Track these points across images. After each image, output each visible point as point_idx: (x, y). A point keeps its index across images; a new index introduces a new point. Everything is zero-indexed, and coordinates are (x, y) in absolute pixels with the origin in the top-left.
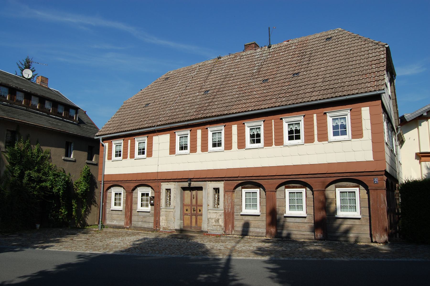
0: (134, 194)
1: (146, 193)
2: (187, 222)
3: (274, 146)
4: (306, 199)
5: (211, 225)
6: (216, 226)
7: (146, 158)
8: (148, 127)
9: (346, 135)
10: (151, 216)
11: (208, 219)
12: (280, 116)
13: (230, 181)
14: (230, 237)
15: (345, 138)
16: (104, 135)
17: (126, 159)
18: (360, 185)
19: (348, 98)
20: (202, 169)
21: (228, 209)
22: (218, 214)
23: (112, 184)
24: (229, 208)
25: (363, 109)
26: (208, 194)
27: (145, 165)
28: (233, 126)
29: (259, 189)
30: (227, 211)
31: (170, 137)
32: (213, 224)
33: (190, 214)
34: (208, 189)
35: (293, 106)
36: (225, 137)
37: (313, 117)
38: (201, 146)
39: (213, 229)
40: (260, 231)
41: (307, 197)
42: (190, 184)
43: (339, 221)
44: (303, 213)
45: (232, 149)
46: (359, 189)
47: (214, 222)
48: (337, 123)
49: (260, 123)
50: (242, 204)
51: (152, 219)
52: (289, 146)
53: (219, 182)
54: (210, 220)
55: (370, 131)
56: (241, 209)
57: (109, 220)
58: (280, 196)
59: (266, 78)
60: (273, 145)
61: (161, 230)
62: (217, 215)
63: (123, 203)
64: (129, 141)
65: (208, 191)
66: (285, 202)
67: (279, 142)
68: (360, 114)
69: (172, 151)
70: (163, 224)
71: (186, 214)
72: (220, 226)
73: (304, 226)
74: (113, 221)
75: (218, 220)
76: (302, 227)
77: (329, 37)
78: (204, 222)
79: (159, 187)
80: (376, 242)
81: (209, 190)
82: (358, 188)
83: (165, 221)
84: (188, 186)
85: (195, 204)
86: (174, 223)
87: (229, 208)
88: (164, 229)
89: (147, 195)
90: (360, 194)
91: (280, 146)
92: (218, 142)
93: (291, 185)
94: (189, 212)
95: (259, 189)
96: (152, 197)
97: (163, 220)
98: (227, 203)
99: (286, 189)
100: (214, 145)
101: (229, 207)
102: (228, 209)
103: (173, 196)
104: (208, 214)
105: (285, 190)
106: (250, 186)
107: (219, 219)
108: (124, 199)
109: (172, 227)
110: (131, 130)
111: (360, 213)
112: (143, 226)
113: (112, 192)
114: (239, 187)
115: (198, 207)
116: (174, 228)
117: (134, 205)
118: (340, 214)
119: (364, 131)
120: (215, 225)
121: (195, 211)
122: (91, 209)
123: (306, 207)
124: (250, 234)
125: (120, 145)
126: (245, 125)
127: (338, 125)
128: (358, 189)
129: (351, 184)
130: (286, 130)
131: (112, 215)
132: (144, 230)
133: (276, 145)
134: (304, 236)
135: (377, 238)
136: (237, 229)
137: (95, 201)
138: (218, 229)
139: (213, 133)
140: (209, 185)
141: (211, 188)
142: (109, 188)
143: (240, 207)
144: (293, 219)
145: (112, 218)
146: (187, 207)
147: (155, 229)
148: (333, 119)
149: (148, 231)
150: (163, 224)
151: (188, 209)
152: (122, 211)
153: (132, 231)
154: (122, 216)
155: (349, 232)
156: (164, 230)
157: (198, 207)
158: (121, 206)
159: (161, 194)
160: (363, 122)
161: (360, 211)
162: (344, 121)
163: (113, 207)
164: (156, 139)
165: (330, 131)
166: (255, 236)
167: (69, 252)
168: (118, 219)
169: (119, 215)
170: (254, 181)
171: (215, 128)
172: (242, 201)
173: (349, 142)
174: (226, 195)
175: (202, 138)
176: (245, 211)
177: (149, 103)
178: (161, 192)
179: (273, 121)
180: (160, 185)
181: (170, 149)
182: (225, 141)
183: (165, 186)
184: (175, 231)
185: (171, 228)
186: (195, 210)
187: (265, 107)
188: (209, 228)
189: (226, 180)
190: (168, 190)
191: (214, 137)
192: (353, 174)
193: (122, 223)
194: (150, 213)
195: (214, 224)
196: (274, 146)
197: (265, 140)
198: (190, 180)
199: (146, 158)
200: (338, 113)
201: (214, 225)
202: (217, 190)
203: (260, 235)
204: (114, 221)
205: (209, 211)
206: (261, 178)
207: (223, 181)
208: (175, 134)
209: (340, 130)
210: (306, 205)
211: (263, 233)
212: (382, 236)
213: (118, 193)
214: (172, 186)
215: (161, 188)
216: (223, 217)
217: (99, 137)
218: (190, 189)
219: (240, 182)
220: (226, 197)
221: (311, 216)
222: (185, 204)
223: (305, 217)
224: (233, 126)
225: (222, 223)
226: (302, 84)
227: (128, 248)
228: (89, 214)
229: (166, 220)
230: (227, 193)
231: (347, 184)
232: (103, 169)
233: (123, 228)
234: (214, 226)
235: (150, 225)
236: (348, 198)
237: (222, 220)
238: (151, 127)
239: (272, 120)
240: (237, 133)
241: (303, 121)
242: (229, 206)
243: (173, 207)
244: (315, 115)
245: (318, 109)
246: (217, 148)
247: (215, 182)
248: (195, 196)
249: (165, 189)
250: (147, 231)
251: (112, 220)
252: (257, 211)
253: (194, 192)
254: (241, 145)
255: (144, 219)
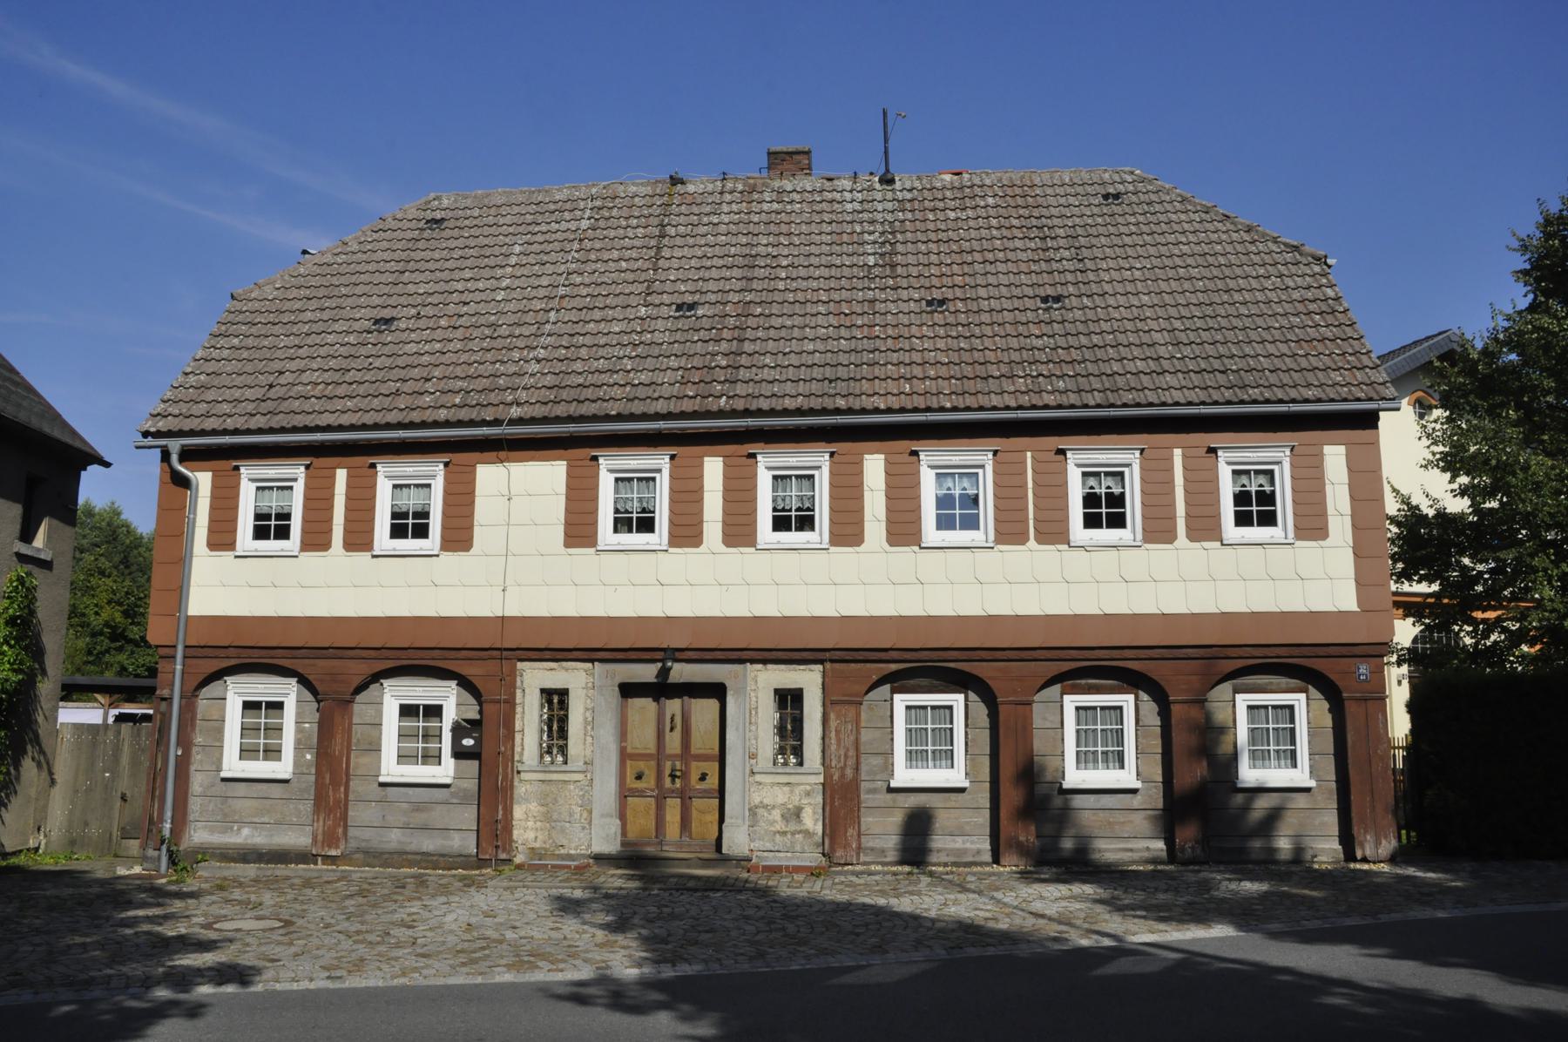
0: (356, 708)
1: (425, 706)
2: (643, 822)
3: (1032, 543)
4: (1136, 730)
5: (766, 831)
6: (789, 836)
7: (438, 556)
8: (447, 424)
9: (978, 528)
10: (455, 801)
11: (753, 811)
12: (1213, 439)
13: (853, 665)
14: (857, 874)
15: (1272, 537)
16: (192, 433)
17: (857, 548)
18: (1310, 687)
19: (1294, 411)
20: (728, 615)
21: (843, 769)
22: (798, 790)
23: (233, 662)
24: (845, 765)
25: (1327, 449)
26: (753, 712)
27: (486, 583)
28: (706, 459)
29: (962, 696)
30: (836, 777)
31: (569, 476)
32: (773, 829)
33: (653, 790)
34: (753, 694)
35: (1112, 413)
36: (306, 508)
37: (1170, 459)
38: (720, 524)
39: (776, 848)
40: (968, 845)
41: (1141, 723)
42: (664, 672)
43: (1239, 799)
44: (1125, 777)
45: (863, 546)
46: (1308, 699)
47: (778, 818)
48: (1244, 486)
49: (980, 458)
50: (892, 750)
51: (467, 816)
52: (1088, 549)
53: (802, 667)
54: (761, 811)
55: (1348, 521)
56: (889, 769)
57: (206, 827)
58: (1045, 719)
59: (387, 313)
60: (1028, 540)
61: (519, 859)
62: (792, 792)
63: (295, 748)
64: (341, 475)
65: (754, 699)
66: (1063, 740)
67: (1053, 532)
68: (860, 473)
69: (579, 531)
70: (531, 835)
71: (640, 794)
72: (807, 834)
73: (1131, 822)
74: (232, 828)
75: (797, 813)
76: (1123, 823)
77: (439, 217)
78: (733, 821)
79: (509, 684)
80: (1365, 860)
81: (757, 697)
82: (1304, 695)
83: (539, 824)
84: (655, 681)
85: (678, 751)
86: (584, 828)
87: (845, 765)
88: (535, 854)
89: (434, 711)
90: (1308, 712)
91: (1202, 543)
92: (797, 510)
93: (1083, 682)
94: (649, 782)
95: (962, 696)
96: (464, 720)
97: (527, 820)
98: (839, 744)
99: (1065, 697)
100: (781, 524)
101: (845, 761)
102: (843, 769)
103: (581, 719)
104: (752, 790)
105: (1062, 698)
106: (924, 682)
107: (803, 808)
108: (299, 730)
109: (573, 845)
110: (527, 420)
111: (1311, 772)
112: (413, 847)
113: (230, 695)
114: (881, 688)
115: (694, 764)
116: (587, 850)
117: (357, 757)
118: (1249, 774)
119: (1330, 518)
120: (784, 833)
121: (679, 777)
122: (18, 778)
123: (1137, 758)
124: (933, 858)
125: (282, 488)
126: (922, 457)
127: (1248, 493)
128: (1302, 696)
129: (1284, 681)
130: (1227, 489)
131: (230, 800)
132: (424, 865)
133: (1040, 541)
134: (1130, 854)
135: (1366, 847)
136: (870, 844)
137: (37, 741)
138: (798, 848)
139: (395, 486)
140: (756, 676)
141: (764, 688)
142: (377, 677)
143: (886, 761)
144: (1092, 797)
145: (225, 815)
146: (641, 765)
147: (488, 857)
148: (937, 474)
149: (449, 869)
150: (531, 835)
151: (647, 772)
152: (286, 781)
153: (375, 872)
154: (291, 806)
155: (1275, 834)
156: (532, 859)
157: (694, 764)
158: (280, 760)
159: (519, 709)
160: (867, 495)
161: (1311, 767)
162: (972, 486)
163: (233, 764)
164: (490, 476)
165: (1076, 511)
166: (955, 864)
167: (376, 988)
168: (266, 819)
169: (270, 802)
170: (952, 665)
171: (408, 469)
172: (892, 739)
173: (823, 554)
174: (832, 716)
175: (727, 490)
176: (904, 776)
177: (393, 319)
178: (518, 701)
179: (1029, 454)
180: (513, 673)
181: (568, 524)
182: (305, 521)
183: (534, 678)
184: (591, 861)
185: (572, 852)
186: (678, 774)
187: (1003, 400)
188: (756, 845)
189: (832, 661)
190: (556, 699)
191: (780, 490)
192: (1296, 651)
193: (297, 838)
194: (452, 789)
195: (780, 826)
196: (1032, 543)
197: (304, 532)
198: (676, 654)
199: (438, 556)
200: (1255, 455)
201: (779, 832)
202: (789, 700)
203: (970, 859)
204: (239, 829)
205: (758, 778)
206: (984, 654)
207: (821, 662)
208: (236, 472)
209: (1104, 510)
210: (1137, 749)
211: (979, 852)
212: (1384, 842)
213: (260, 703)
214: (574, 677)
215: (519, 683)
216: (819, 799)
217: (164, 443)
218: (661, 690)
219: (894, 667)
220: (833, 724)
221: (1156, 787)
222: (629, 750)
223: (1134, 791)
224: (866, 456)
225: (812, 821)
226: (459, 358)
227: (1057, 947)
228: (10, 801)
229: (547, 817)
230: (838, 707)
231: (1271, 683)
232: (179, 591)
233: (304, 857)
234: (778, 836)
235: (450, 843)
236: (1099, 727)
237: (814, 813)
238: (472, 423)
239: (1171, 448)
240: (883, 486)
241: (826, 470)
242: (846, 756)
243: (579, 765)
244: (1178, 453)
245: (1188, 433)
246: (409, 544)
247: (783, 667)
248: (678, 720)
249: (538, 692)
250: (443, 869)
251: (229, 821)
252: (954, 776)
253: (674, 706)
254: (903, 530)
255: (419, 819)
